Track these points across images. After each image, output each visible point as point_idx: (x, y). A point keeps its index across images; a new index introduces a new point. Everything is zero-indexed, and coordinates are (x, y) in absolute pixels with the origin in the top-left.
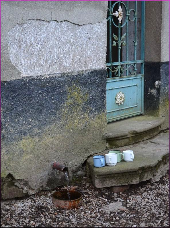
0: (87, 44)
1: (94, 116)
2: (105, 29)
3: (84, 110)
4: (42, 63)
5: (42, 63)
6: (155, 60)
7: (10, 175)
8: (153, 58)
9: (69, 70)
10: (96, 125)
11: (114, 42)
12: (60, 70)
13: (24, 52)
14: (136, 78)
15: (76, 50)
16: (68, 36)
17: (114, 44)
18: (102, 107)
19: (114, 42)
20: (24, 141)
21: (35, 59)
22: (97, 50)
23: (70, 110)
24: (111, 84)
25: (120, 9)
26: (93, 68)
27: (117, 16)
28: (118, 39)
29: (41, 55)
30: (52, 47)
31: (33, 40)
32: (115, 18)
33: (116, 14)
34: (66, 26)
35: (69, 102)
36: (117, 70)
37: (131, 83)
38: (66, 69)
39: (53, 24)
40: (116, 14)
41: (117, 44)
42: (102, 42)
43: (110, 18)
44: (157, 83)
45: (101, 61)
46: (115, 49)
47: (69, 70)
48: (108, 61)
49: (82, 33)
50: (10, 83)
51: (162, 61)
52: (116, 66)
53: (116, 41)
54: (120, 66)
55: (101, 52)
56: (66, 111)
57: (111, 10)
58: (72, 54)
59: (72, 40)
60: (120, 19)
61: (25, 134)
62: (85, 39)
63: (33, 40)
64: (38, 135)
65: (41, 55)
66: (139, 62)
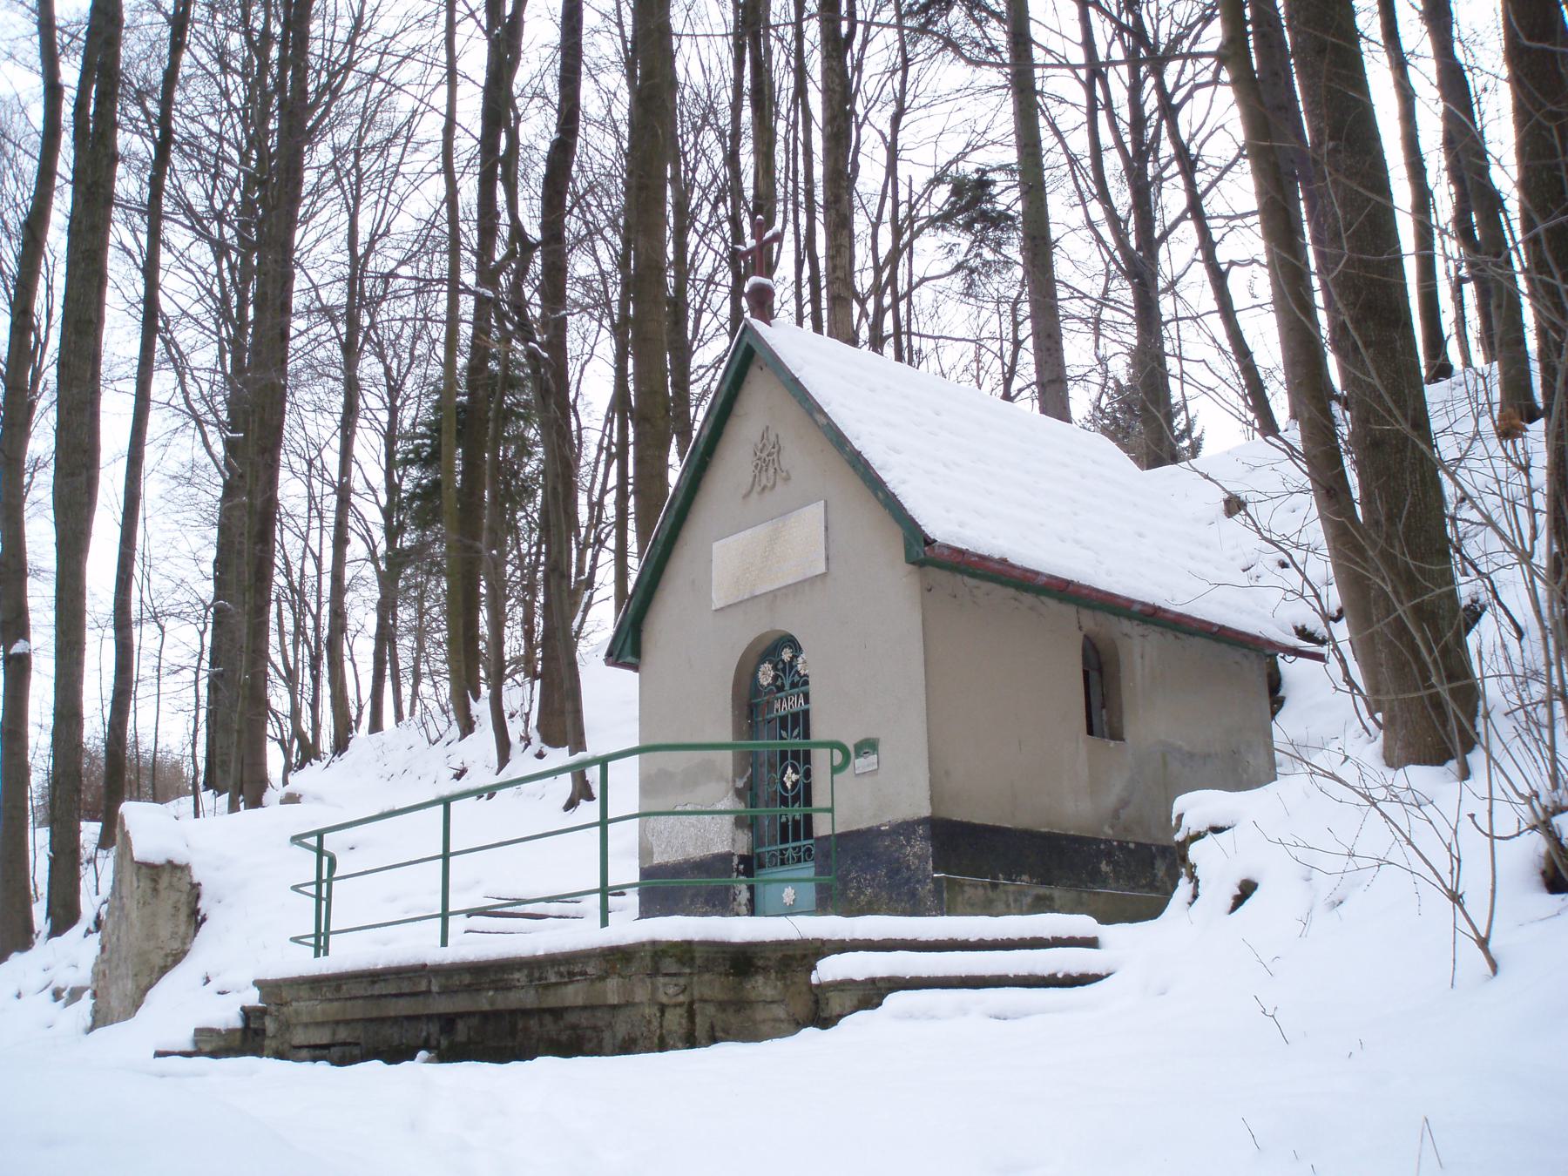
33: (794, 777)
40: (794, 777)
52: (786, 849)
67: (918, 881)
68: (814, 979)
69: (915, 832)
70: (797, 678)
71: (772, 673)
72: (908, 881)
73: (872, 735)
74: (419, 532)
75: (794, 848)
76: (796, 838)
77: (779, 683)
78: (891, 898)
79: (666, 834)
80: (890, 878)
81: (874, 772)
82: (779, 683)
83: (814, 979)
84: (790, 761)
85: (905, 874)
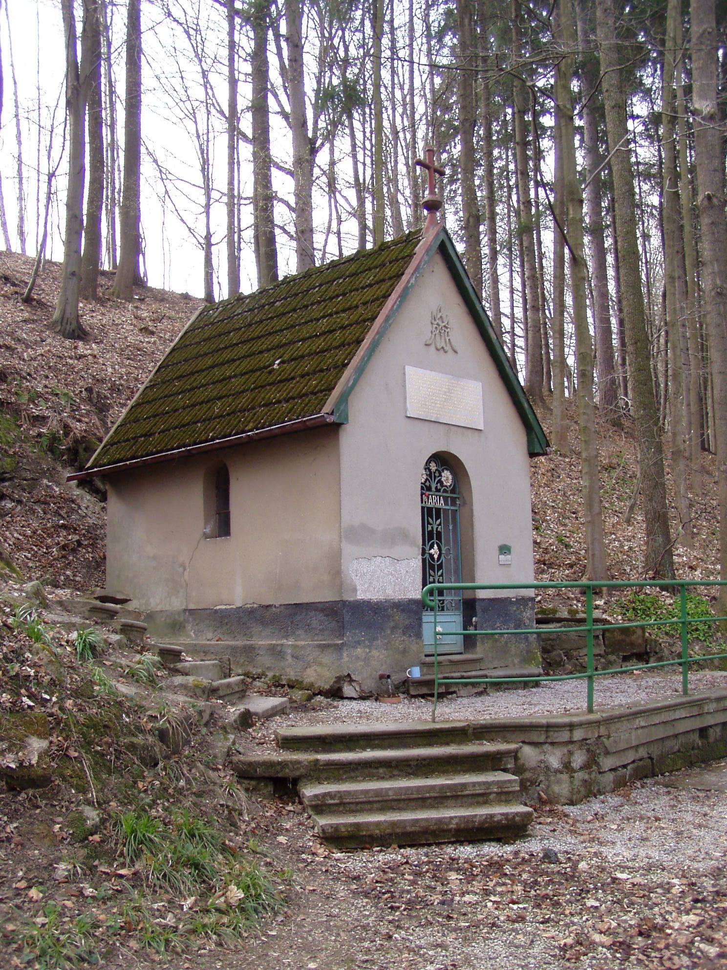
2: (420, 564)
3: (404, 633)
5: (371, 589)
7: (349, 675)
10: (414, 649)
14: (38, 216)
17: (430, 528)
18: (419, 635)
23: (392, 632)
24: (427, 617)
29: (371, 583)
32: (431, 556)
35: (392, 624)
37: (448, 619)
40: (432, 551)
43: (427, 556)
44: (474, 619)
46: (431, 533)
49: (402, 567)
50: (350, 602)
56: (389, 632)
57: (427, 548)
60: (436, 556)
62: (403, 572)
64: (369, 647)
65: (371, 583)
66: (456, 598)
71: (445, 483)
77: (428, 484)
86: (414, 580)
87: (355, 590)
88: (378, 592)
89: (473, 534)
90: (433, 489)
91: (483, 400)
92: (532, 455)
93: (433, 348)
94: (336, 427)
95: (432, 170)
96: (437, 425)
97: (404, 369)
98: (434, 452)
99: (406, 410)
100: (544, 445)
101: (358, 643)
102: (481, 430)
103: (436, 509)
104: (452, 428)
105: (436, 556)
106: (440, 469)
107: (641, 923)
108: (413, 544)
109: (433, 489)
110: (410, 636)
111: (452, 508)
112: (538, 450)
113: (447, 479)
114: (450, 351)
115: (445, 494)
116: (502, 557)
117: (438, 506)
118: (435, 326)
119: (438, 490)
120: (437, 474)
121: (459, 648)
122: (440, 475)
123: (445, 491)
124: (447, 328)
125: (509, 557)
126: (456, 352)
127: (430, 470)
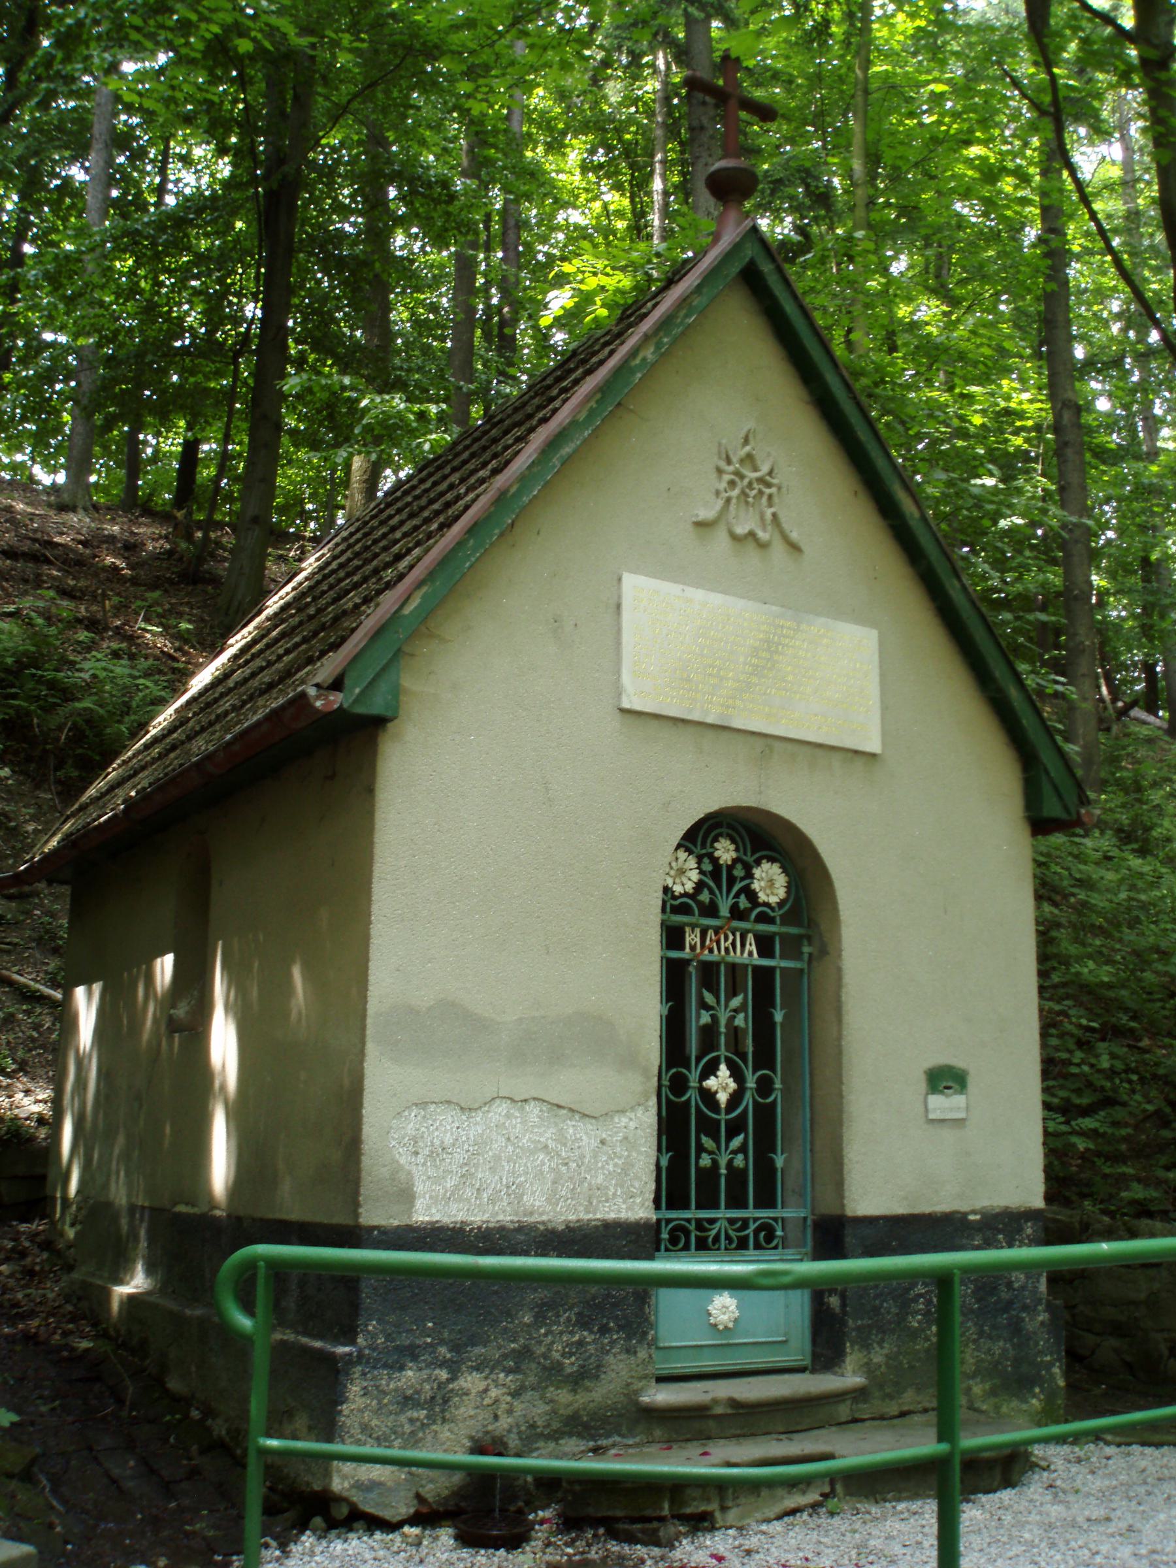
0: (595, 1156)
1: (613, 1343)
3: (583, 1322)
4: (468, 1192)
6: (836, 1211)
8: (828, 1208)
9: (541, 1214)
11: (704, 1155)
12: (517, 1214)
13: (424, 1164)
15: (564, 1169)
16: (541, 1135)
17: (705, 1018)
19: (704, 1155)
20: (410, 1373)
21: (450, 1183)
22: (625, 1171)
25: (723, 1071)
26: (612, 1216)
27: (714, 1089)
28: (719, 1148)
30: (497, 1158)
31: (448, 1140)
33: (711, 1083)
34: (536, 1111)
36: (714, 1232)
38: (531, 1214)
39: (502, 1108)
40: (711, 1083)
41: (715, 1163)
42: (640, 1153)
45: (638, 1200)
47: (541, 1214)
48: (657, 1202)
51: (849, 1212)
52: (712, 1221)
53: (710, 1153)
54: (725, 1223)
55: (637, 1178)
58: (550, 1177)
59: (551, 1144)
60: (723, 1097)
61: (415, 1358)
63: (448, 1140)
67: (1025, 1308)
68: (14, 1418)
69: (1020, 1230)
70: (743, 903)
71: (762, 897)
72: (1010, 1303)
73: (959, 1063)
74: (93, 44)
75: (732, 1221)
76: (736, 1201)
77: (705, 897)
78: (981, 1333)
79: (460, 1156)
80: (978, 1301)
81: (959, 1123)
82: (705, 897)
83: (14, 1418)
84: (723, 1052)
85: (1005, 1295)
86: (627, 1167)
87: (407, 1196)
88: (492, 1200)
89: (839, 1038)
90: (724, 911)
91: (883, 676)
92: (1039, 825)
93: (721, 535)
94: (375, 725)
95: (733, 103)
96: (725, 735)
97: (620, 579)
98: (713, 806)
99: (619, 692)
100: (1071, 798)
101: (412, 1353)
102: (873, 756)
103: (727, 964)
104: (777, 745)
105: (723, 1097)
106: (750, 859)
107: (1046, 236)
108: (628, 1061)
109: (724, 911)
110: (604, 1330)
111: (785, 964)
112: (1052, 808)
113: (771, 882)
114: (778, 547)
115: (762, 927)
116: (935, 1101)
117: (738, 957)
118: (727, 477)
119: (737, 913)
120: (739, 872)
121: (799, 1349)
122: (750, 875)
123: (763, 918)
124: (769, 485)
125: (959, 1100)
126: (795, 547)
127: (715, 861)
